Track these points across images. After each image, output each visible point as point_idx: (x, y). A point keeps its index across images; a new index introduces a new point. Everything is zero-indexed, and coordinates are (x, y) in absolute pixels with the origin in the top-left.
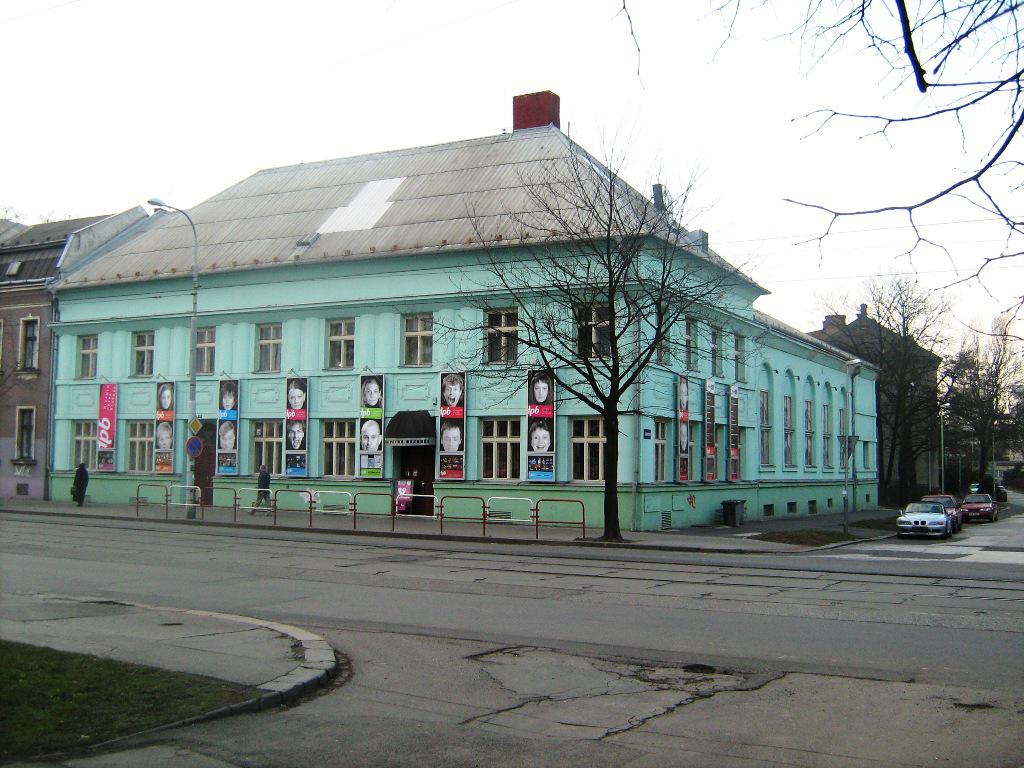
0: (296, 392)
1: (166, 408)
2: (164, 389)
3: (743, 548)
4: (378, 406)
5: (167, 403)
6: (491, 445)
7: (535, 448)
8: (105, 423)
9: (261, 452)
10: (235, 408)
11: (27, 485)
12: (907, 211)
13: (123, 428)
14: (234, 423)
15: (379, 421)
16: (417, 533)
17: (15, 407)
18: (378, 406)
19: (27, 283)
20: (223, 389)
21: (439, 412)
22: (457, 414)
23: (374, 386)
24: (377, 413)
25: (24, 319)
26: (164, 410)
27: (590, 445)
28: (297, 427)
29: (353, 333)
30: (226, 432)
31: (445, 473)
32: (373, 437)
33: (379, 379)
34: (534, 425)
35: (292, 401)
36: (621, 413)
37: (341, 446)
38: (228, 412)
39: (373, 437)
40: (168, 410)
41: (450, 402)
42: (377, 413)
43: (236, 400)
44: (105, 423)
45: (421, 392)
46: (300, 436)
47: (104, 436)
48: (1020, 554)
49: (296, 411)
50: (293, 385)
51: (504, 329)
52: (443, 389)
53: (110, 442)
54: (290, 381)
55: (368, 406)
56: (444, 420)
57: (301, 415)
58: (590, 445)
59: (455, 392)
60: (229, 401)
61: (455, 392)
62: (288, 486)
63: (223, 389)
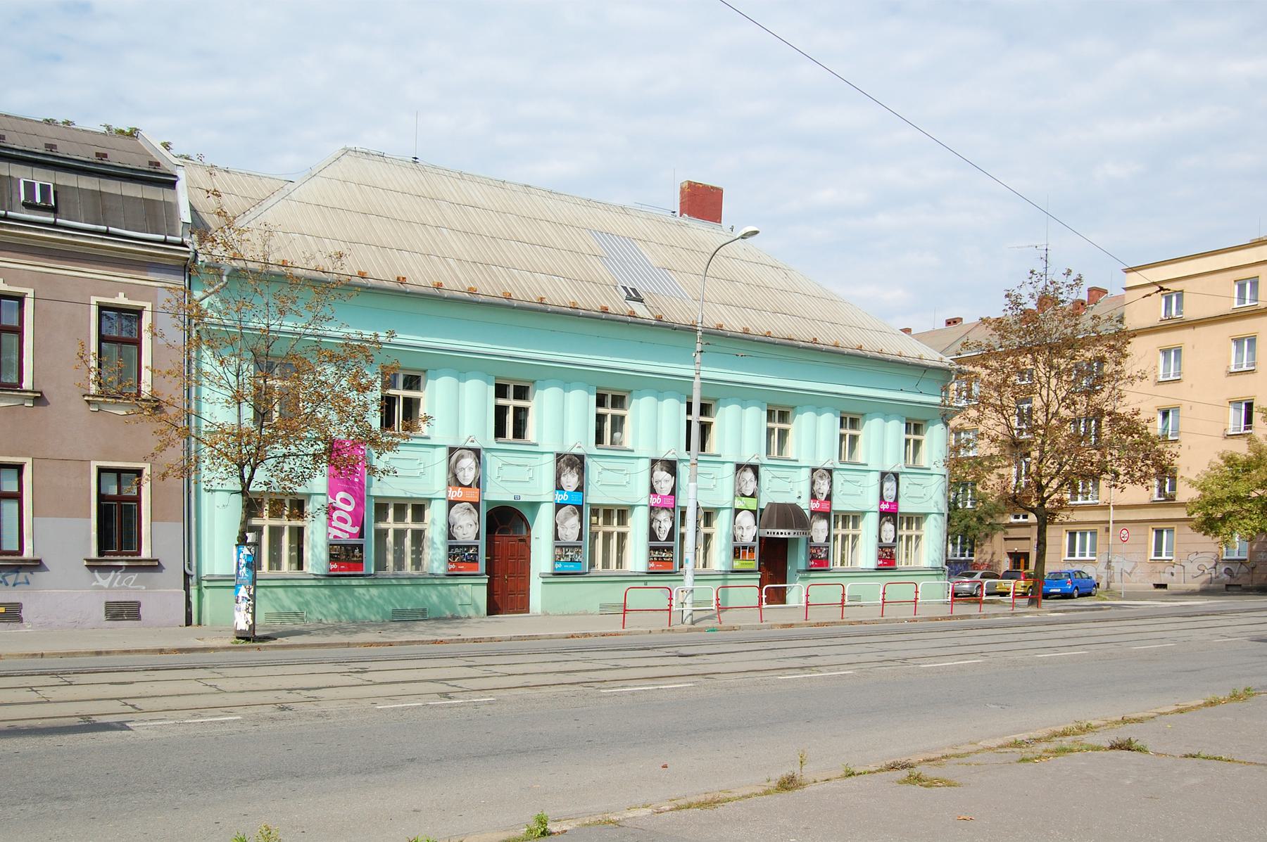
0: (662, 476)
2: (461, 457)
3: (126, 656)
4: (753, 496)
5: (468, 476)
6: (386, 532)
9: (279, 549)
10: (580, 489)
11: (138, 604)
13: (369, 513)
14: (580, 508)
15: (754, 512)
16: (306, 650)
18: (753, 496)
19: (107, 233)
20: (562, 464)
21: (805, 504)
22: (825, 507)
23: (749, 475)
24: (752, 504)
27: (272, 529)
28: (663, 515)
30: (566, 519)
31: (335, 566)
32: (748, 528)
33: (755, 469)
35: (657, 487)
37: (399, 534)
39: (748, 528)
40: (470, 486)
41: (819, 496)
42: (752, 504)
43: (581, 478)
45: (509, 473)
49: (662, 497)
50: (658, 466)
52: (813, 483)
53: (356, 530)
54: (654, 462)
55: (743, 495)
56: (813, 513)
57: (669, 502)
58: (272, 529)
59: (823, 487)
60: (570, 480)
61: (889, 492)
62: (646, 581)
63: (562, 464)
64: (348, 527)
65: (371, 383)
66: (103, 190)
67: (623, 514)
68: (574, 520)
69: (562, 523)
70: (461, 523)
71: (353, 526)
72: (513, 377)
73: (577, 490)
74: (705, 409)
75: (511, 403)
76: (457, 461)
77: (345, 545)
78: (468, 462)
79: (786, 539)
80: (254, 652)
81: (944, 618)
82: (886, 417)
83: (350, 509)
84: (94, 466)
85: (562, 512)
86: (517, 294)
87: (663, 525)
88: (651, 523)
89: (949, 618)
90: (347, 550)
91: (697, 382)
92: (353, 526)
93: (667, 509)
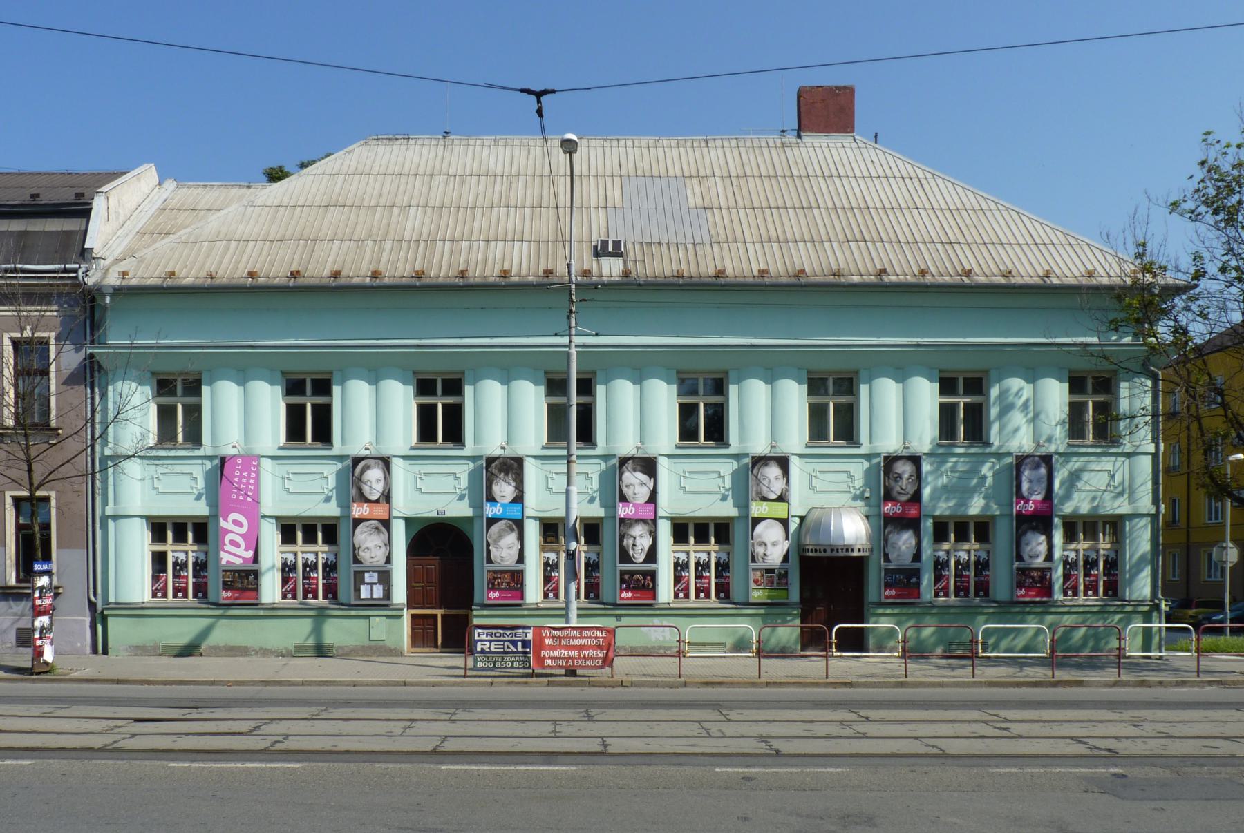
1: (374, 498)
2: (367, 467)
4: (782, 498)
7: (1026, 557)
8: (236, 523)
12: (534, 98)
15: (785, 523)
17: (3, 492)
19: (15, 270)
25: (53, 341)
26: (368, 501)
29: (942, 405)
30: (500, 537)
32: (774, 544)
34: (1024, 526)
36: (264, 517)
38: (903, 504)
40: (377, 501)
44: (236, 523)
46: (645, 543)
47: (233, 543)
48: (1236, 714)
49: (636, 506)
51: (962, 401)
53: (250, 554)
55: (765, 499)
57: (647, 513)
63: (493, 469)
64: (240, 551)
65: (1021, 389)
66: (29, 229)
67: (1116, 525)
68: (512, 538)
69: (496, 542)
70: (368, 544)
71: (246, 549)
72: (307, 368)
73: (648, 502)
74: (586, 387)
75: (440, 402)
76: (362, 472)
77: (239, 571)
78: (905, 469)
79: (861, 558)
80: (28, 685)
81: (816, 685)
82: (771, 377)
83: (244, 530)
84: (8, 496)
85: (495, 528)
86: (476, 273)
87: (638, 541)
88: (621, 540)
89: (901, 685)
90: (240, 577)
91: (574, 351)
92: (246, 549)
93: (644, 521)
